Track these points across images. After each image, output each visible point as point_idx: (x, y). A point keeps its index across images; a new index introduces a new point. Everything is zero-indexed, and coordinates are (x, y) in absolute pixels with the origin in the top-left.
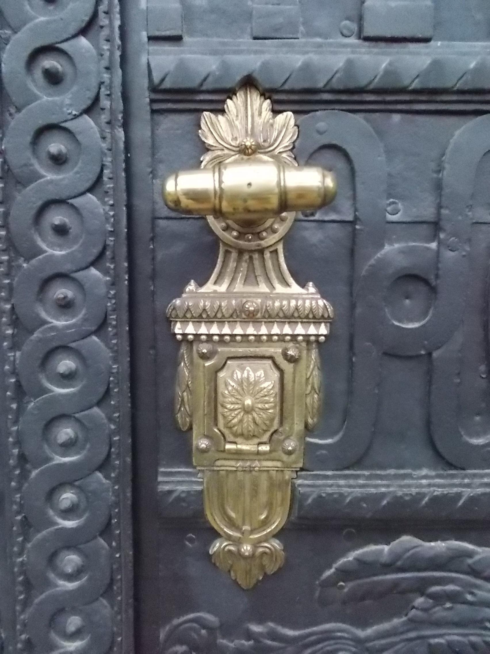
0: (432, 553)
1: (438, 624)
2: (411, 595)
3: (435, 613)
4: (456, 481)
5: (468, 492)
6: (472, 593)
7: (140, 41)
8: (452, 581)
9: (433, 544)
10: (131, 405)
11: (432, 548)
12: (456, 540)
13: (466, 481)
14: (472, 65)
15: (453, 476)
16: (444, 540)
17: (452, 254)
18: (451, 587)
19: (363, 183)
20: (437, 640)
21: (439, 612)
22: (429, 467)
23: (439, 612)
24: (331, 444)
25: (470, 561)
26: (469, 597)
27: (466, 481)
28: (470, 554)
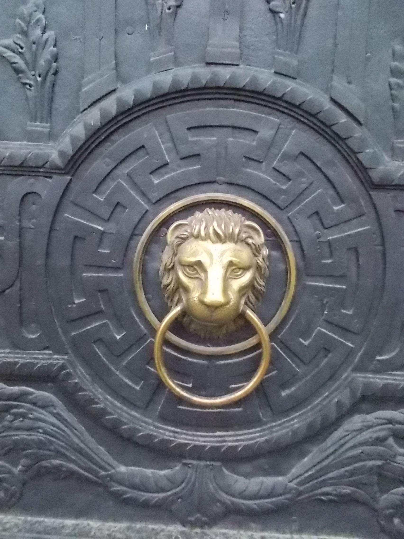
0: (10, 392)
1: (18, 429)
2: (3, 414)
3: (15, 423)
4: (19, 356)
5: (22, 361)
6: (32, 414)
7: (244, 80)
8: (22, 407)
9: (12, 388)
10: (281, 394)
11: (11, 390)
12: (26, 387)
13: (25, 356)
14: (7, 154)
15: (18, 353)
16: (18, 386)
17: (12, 242)
18: (21, 410)
19: (298, 225)
20: (16, 437)
21: (17, 423)
22: (10, 348)
23: (17, 423)
24: (246, 396)
25: (30, 397)
26: (31, 416)
27: (25, 356)
28: (31, 394)
